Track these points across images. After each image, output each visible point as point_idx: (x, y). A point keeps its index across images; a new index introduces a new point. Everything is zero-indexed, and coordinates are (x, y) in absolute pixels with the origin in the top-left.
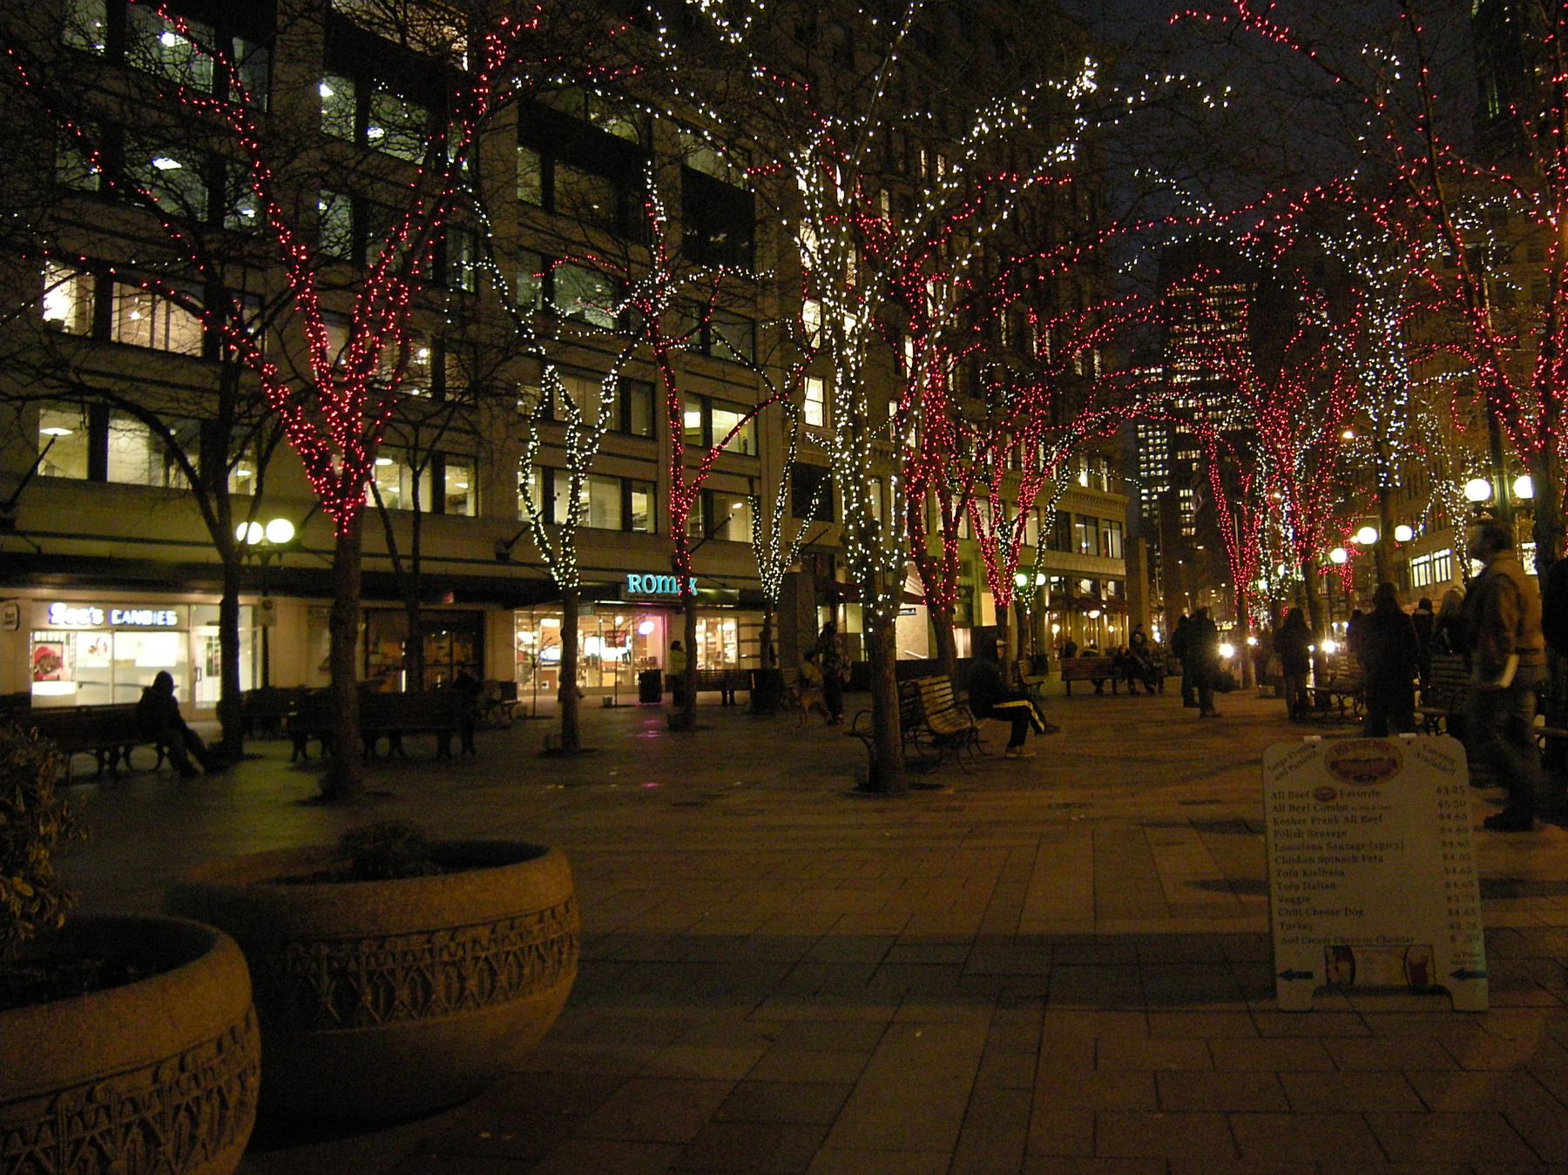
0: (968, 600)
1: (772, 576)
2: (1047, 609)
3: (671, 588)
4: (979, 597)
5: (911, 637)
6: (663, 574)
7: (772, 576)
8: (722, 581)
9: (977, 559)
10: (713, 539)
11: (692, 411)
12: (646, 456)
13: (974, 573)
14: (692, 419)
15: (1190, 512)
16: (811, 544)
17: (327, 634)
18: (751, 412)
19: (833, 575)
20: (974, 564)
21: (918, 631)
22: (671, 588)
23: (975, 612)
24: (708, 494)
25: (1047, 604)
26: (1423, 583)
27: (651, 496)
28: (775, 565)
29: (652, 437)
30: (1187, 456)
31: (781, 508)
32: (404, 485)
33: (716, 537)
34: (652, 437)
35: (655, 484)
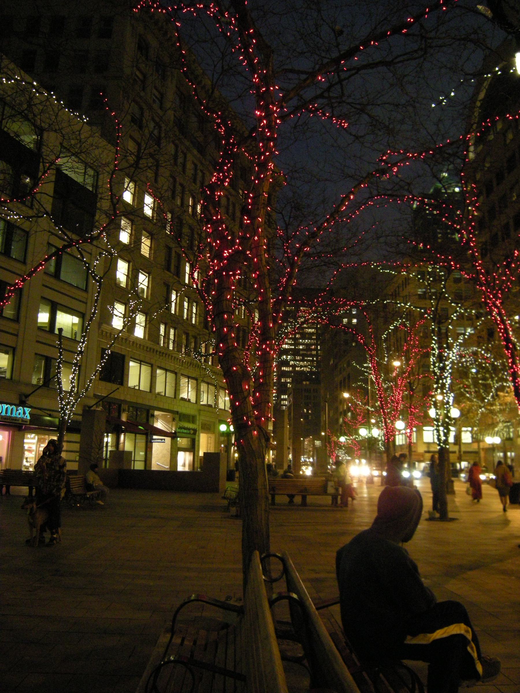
0: (193, 436)
1: (68, 403)
2: (233, 445)
3: (12, 413)
4: (199, 436)
5: (161, 455)
6: (7, 404)
7: (68, 403)
8: (49, 412)
9: (200, 415)
10: (48, 387)
11: (43, 311)
12: (11, 331)
13: (197, 422)
14: (43, 317)
15: (285, 405)
16: (107, 396)
17: (254, 449)
18: (82, 315)
19: (119, 416)
20: (198, 417)
21: (165, 452)
22: (12, 413)
23: (196, 442)
24: (48, 360)
25: (233, 442)
26: (401, 443)
27: (11, 355)
28: (71, 396)
29: (16, 320)
30: (286, 380)
31: (81, 352)
32: (138, 445)
33: (50, 386)
34: (16, 320)
35: (14, 349)
